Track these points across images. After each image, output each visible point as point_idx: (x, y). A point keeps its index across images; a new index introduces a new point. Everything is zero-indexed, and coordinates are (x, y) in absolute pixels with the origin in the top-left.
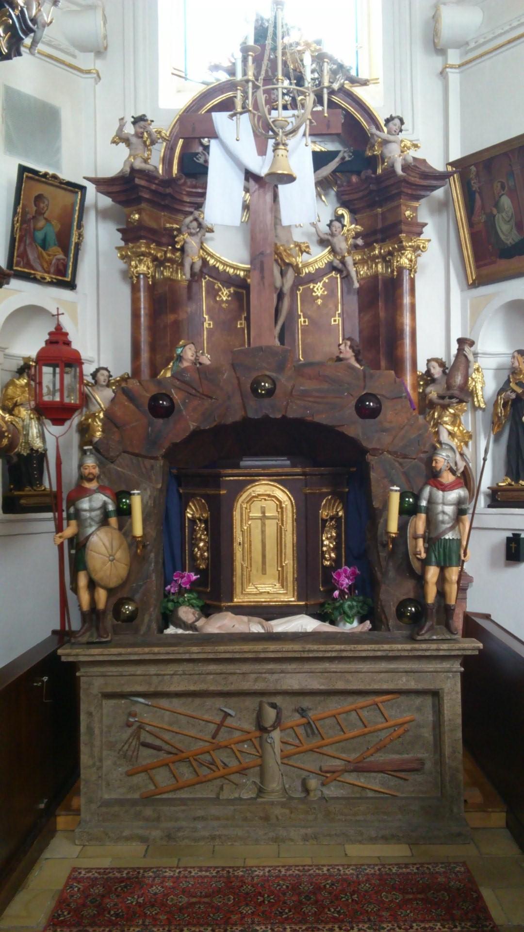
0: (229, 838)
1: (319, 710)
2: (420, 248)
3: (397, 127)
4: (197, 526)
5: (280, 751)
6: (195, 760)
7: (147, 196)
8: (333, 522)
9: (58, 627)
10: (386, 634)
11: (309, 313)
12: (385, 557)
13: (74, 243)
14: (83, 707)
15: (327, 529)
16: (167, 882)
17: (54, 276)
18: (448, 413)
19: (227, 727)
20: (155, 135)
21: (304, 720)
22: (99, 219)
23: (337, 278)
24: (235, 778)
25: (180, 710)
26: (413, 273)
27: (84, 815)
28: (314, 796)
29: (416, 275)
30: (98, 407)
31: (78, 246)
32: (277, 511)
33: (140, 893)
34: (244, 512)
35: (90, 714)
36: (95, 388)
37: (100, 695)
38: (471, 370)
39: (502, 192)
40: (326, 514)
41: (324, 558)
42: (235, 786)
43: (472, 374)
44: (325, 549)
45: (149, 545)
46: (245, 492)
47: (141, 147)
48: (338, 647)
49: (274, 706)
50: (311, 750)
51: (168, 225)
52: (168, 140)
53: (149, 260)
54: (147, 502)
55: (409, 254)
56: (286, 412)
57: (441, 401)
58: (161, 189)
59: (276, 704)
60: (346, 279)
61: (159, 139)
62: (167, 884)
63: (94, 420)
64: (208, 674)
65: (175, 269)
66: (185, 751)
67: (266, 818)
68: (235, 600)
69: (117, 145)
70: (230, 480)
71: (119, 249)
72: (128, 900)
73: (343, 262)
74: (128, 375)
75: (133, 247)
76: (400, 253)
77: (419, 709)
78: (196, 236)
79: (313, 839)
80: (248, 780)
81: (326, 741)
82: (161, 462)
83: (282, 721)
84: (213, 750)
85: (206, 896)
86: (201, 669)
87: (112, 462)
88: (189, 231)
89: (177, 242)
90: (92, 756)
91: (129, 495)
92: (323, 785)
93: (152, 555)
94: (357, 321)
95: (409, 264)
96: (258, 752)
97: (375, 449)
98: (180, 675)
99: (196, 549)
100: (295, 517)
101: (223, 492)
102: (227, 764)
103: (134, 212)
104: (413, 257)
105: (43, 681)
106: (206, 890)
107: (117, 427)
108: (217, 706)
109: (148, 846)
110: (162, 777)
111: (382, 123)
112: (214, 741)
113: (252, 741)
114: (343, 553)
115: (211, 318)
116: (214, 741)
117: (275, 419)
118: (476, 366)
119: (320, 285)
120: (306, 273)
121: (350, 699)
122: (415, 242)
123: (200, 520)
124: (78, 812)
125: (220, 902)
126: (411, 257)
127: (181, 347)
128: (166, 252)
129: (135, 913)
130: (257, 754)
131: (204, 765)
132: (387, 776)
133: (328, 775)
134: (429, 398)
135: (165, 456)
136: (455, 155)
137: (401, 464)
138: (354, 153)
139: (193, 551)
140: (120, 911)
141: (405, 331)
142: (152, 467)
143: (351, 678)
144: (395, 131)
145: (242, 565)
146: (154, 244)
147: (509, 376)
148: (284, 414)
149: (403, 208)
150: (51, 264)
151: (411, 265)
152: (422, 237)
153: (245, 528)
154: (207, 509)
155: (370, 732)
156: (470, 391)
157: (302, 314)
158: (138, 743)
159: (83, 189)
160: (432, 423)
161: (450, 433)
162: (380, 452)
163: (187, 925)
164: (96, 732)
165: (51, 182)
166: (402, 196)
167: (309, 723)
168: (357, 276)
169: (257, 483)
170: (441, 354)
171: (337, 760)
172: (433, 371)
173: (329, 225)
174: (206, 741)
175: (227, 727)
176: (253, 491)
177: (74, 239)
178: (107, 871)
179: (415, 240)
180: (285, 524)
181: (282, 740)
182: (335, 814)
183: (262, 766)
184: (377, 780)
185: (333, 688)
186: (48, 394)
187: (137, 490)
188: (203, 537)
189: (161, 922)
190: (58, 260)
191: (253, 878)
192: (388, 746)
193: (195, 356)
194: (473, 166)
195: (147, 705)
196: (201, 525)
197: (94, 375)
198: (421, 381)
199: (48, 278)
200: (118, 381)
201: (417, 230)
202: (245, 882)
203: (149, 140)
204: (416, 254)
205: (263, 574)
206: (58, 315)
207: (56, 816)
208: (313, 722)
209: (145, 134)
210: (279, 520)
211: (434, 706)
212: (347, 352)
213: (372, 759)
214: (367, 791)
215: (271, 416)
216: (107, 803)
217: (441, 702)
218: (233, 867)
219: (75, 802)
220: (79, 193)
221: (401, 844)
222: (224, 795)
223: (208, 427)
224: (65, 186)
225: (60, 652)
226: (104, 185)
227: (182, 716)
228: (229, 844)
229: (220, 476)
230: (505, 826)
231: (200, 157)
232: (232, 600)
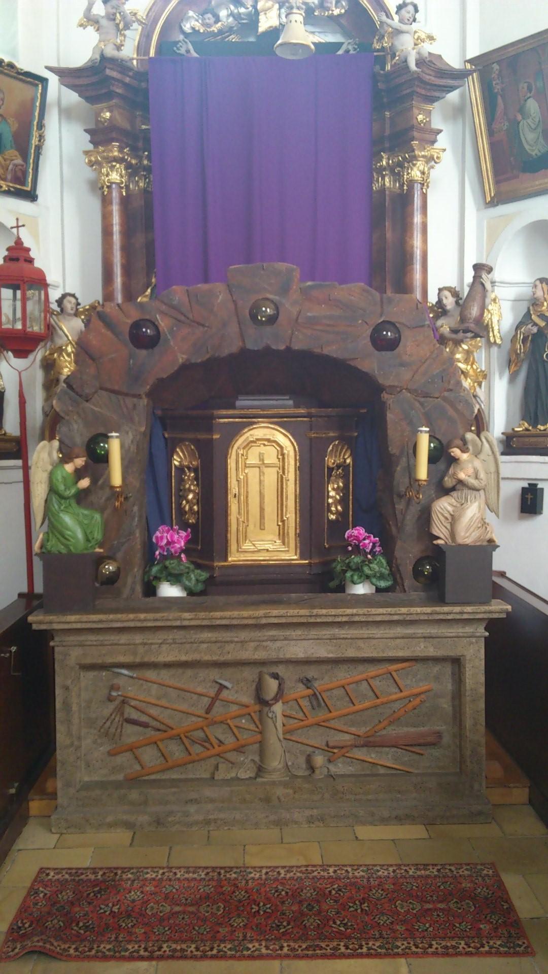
0: (225, 823)
1: (324, 681)
2: (433, 159)
3: (410, 15)
4: (186, 475)
5: (282, 725)
6: (186, 737)
7: (119, 91)
8: (340, 470)
9: (24, 589)
10: (401, 595)
12: (402, 510)
13: (33, 146)
14: (58, 680)
15: (333, 478)
16: (147, 886)
17: (11, 185)
18: (460, 349)
19: (222, 700)
20: (129, 17)
21: (309, 692)
22: (63, 121)
24: (232, 756)
25: (172, 682)
26: (425, 187)
27: (61, 800)
28: (318, 775)
29: (428, 190)
30: (66, 339)
31: (39, 148)
32: (278, 458)
33: (115, 900)
34: (240, 459)
35: (67, 688)
36: (60, 317)
37: (78, 667)
38: (488, 301)
39: (529, 95)
40: (332, 461)
41: (329, 511)
42: (231, 765)
43: (488, 306)
44: (330, 501)
45: (131, 497)
46: (241, 436)
47: (113, 31)
48: (349, 611)
49: (276, 676)
50: (318, 725)
52: (144, 24)
53: (123, 166)
54: (130, 447)
55: (420, 165)
56: (290, 343)
57: (454, 336)
59: (277, 674)
61: (134, 22)
62: (148, 889)
63: (60, 355)
64: (203, 642)
66: (174, 727)
67: (267, 800)
68: (230, 559)
69: (84, 29)
70: (224, 423)
71: (86, 153)
72: (101, 909)
75: (104, 151)
76: (411, 164)
77: (437, 678)
79: (319, 821)
80: (246, 758)
81: (334, 714)
82: (145, 401)
83: (284, 693)
84: (207, 726)
85: (192, 905)
86: (194, 636)
87: (87, 401)
90: (69, 733)
91: (105, 437)
92: (330, 761)
93: (136, 508)
95: (421, 177)
96: (258, 727)
97: (390, 386)
98: (170, 644)
99: (184, 502)
100: (298, 464)
101: (216, 436)
102: (223, 741)
103: (105, 110)
104: (426, 169)
105: (11, 651)
106: (177, 922)
107: (93, 359)
108: (212, 678)
109: (134, 833)
110: (149, 756)
111: (393, 10)
112: (207, 716)
113: (251, 716)
114: (351, 506)
116: (207, 716)
117: (278, 351)
118: (493, 296)
121: (361, 668)
122: (428, 151)
123: (189, 468)
124: (53, 796)
125: (208, 912)
126: (424, 169)
129: (107, 926)
130: (257, 729)
131: (196, 743)
132: (400, 750)
133: (335, 751)
134: (440, 332)
135: (149, 395)
136: (473, 51)
137: (422, 404)
139: (181, 504)
140: (90, 922)
141: (415, 255)
142: (135, 406)
143: (362, 645)
144: (408, 20)
145: (238, 519)
146: (128, 149)
147: (529, 308)
148: (288, 344)
149: (416, 111)
150: (7, 169)
151: (423, 178)
152: (436, 145)
153: (242, 477)
154: (197, 456)
155: (383, 704)
156: (485, 324)
158: (121, 719)
159: (44, 81)
162: (398, 389)
163: (167, 941)
164: (73, 709)
165: (6, 71)
166: (414, 97)
167: (315, 695)
169: (254, 426)
170: (453, 283)
171: (346, 735)
172: (445, 301)
174: (199, 716)
175: (222, 700)
176: (251, 435)
177: (34, 141)
178: (80, 872)
179: (428, 149)
180: (286, 472)
181: (285, 714)
182: (343, 793)
183: (261, 743)
184: (390, 756)
185: (343, 656)
186: (8, 322)
187: (115, 432)
188: (192, 488)
189: (137, 937)
190: (16, 165)
191: (247, 882)
192: (402, 718)
194: (495, 64)
195: (132, 677)
196: (190, 474)
197: (60, 302)
198: (430, 313)
199: (4, 186)
200: (87, 310)
201: (431, 137)
202: (237, 887)
203: (122, 23)
204: (429, 166)
205: (261, 529)
206: (18, 227)
207: (28, 802)
208: (320, 693)
209: (118, 15)
210: (279, 468)
211: (453, 674)
213: (384, 732)
214: (379, 767)
215: (274, 347)
216: (87, 787)
217: (462, 670)
218: (225, 868)
219: (49, 786)
220: (40, 86)
221: (416, 824)
222: (219, 776)
223: (200, 360)
224: (24, 78)
225: (30, 619)
226: (68, 76)
227: (171, 689)
228: (226, 828)
229: (212, 417)
230: (528, 802)
231: (181, 46)
232: (226, 560)
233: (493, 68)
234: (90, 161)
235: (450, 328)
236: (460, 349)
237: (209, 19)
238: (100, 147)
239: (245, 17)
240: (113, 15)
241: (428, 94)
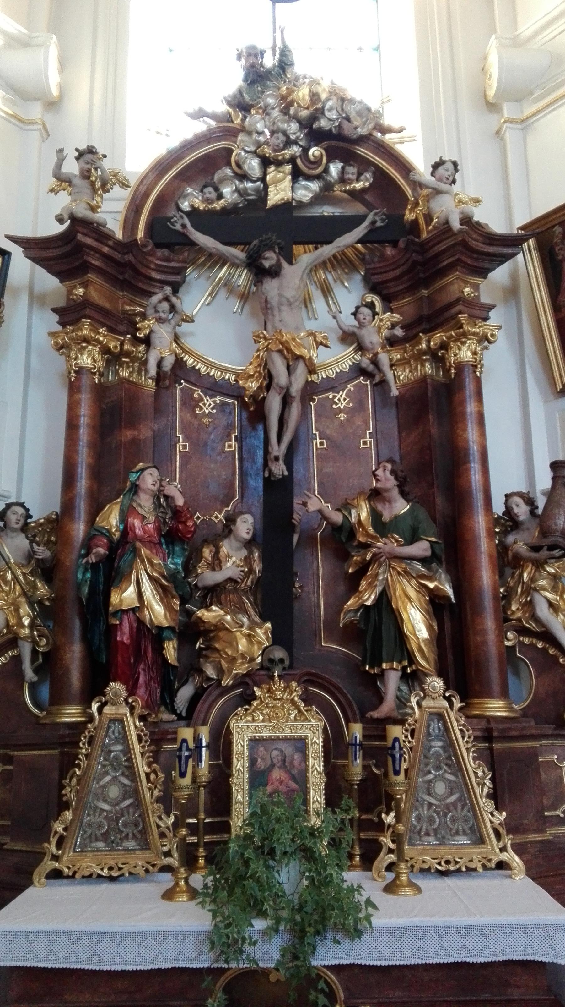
11: (328, 432)
18: (544, 573)
22: (35, 306)
23: (367, 385)
47: (87, 190)
51: (127, 308)
57: (534, 555)
58: (117, 256)
60: (379, 386)
65: (136, 369)
69: (56, 194)
71: (53, 334)
73: (375, 362)
74: (57, 514)
78: (167, 324)
88: (157, 315)
89: (139, 329)
94: (396, 444)
104: (479, 349)
115: (187, 438)
119: (344, 394)
120: (322, 378)
122: (480, 327)
126: (476, 349)
127: (137, 472)
128: (122, 344)
138: (388, 216)
144: (448, 179)
146: (104, 329)
151: (476, 360)
157: (317, 433)
160: (519, 590)
161: (551, 605)
168: (396, 382)
172: (516, 510)
173: (355, 314)
193: (158, 485)
194: (556, 227)
200: (41, 525)
201: (483, 314)
212: (387, 480)
233: (554, 232)
234: (56, 343)
235: (526, 544)
236: (544, 573)
237: (210, 193)
238: (68, 327)
239: (253, 193)
240: (88, 171)
241: (475, 264)
